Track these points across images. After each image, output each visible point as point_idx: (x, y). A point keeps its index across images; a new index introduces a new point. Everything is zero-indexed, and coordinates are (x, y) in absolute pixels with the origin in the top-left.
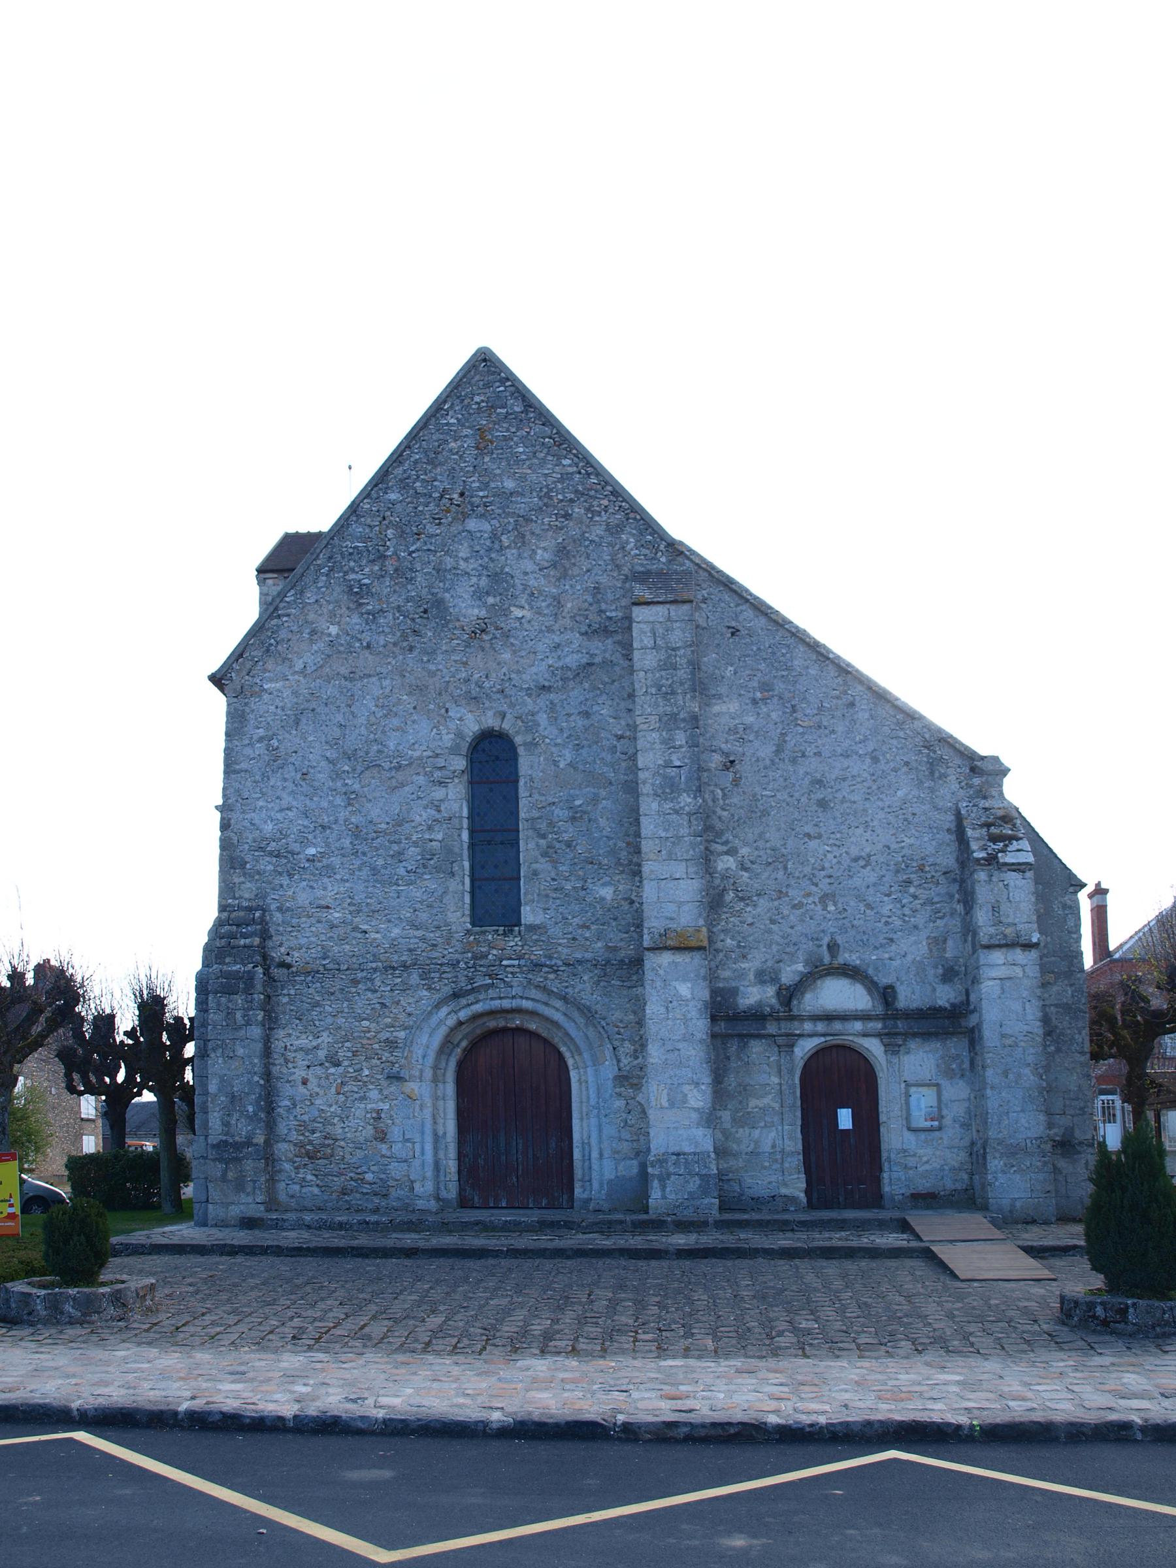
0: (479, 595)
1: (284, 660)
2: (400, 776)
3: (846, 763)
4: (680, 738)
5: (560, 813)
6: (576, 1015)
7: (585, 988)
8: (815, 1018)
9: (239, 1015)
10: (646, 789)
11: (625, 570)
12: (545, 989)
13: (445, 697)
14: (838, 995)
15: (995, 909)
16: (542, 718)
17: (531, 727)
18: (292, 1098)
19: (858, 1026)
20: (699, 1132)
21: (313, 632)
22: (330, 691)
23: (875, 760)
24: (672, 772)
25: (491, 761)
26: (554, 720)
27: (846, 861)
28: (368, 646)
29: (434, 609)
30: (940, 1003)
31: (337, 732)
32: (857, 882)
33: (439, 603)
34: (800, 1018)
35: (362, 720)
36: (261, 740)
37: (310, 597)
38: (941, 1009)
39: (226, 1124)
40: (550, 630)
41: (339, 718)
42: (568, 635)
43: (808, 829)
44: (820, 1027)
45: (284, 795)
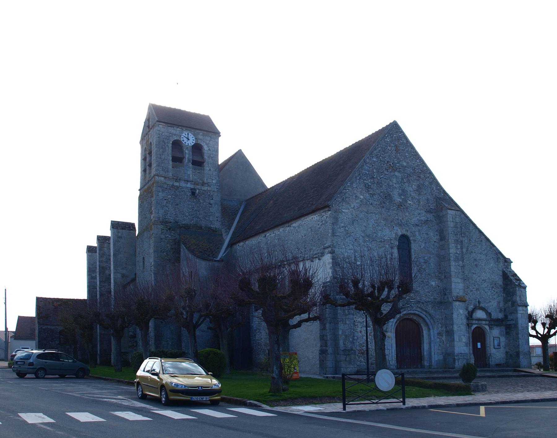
0: (400, 195)
1: (348, 203)
2: (382, 244)
3: (481, 256)
4: (459, 247)
5: (422, 260)
6: (428, 316)
7: (430, 308)
8: (476, 320)
9: (346, 311)
10: (452, 259)
11: (434, 195)
12: (422, 309)
13: (393, 223)
14: (480, 314)
15: (520, 297)
16: (417, 233)
17: (414, 236)
18: (357, 337)
19: (484, 322)
20: (465, 348)
21: (356, 196)
22: (361, 215)
23: (486, 256)
24: (457, 255)
25: (404, 242)
26: (420, 234)
27: (481, 281)
28: (372, 204)
29: (388, 197)
30: (499, 318)
31: (364, 228)
32: (483, 286)
33: (390, 195)
34: (473, 320)
35: (371, 226)
36: (343, 227)
37: (355, 185)
38: (499, 319)
39: (344, 344)
40: (417, 209)
41: (365, 224)
42: (422, 211)
43: (473, 271)
44: (477, 322)
45: (350, 245)
